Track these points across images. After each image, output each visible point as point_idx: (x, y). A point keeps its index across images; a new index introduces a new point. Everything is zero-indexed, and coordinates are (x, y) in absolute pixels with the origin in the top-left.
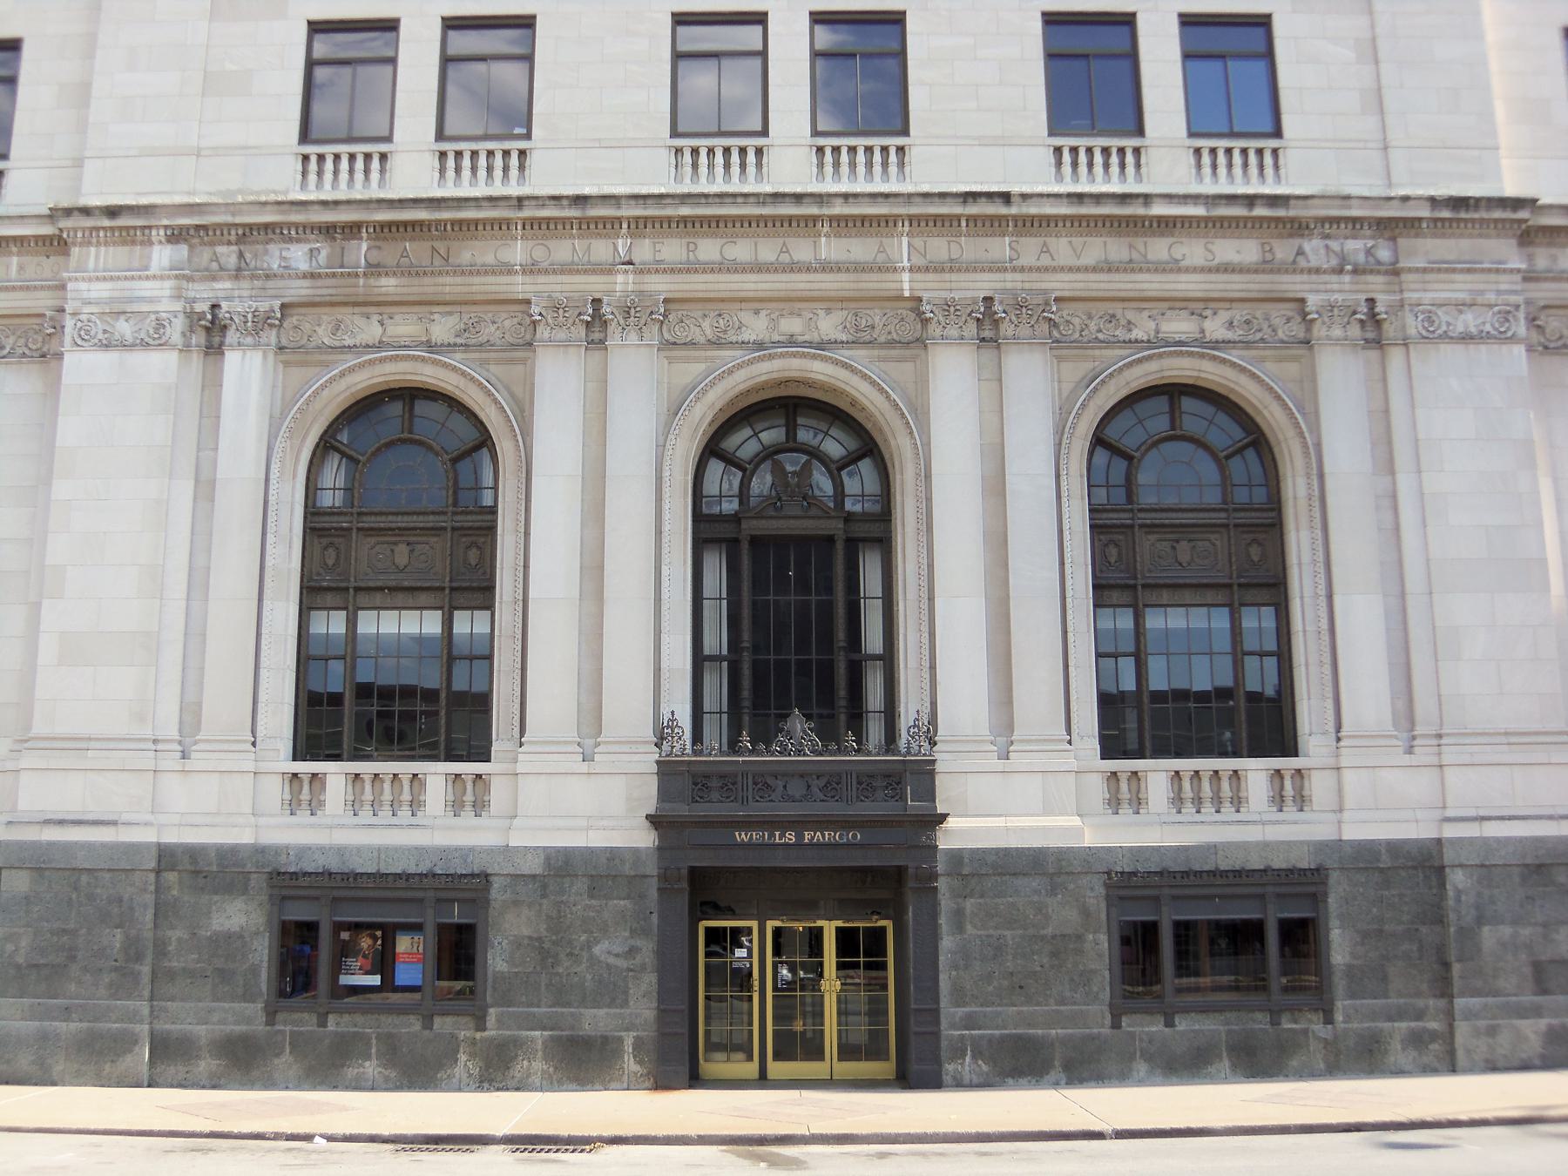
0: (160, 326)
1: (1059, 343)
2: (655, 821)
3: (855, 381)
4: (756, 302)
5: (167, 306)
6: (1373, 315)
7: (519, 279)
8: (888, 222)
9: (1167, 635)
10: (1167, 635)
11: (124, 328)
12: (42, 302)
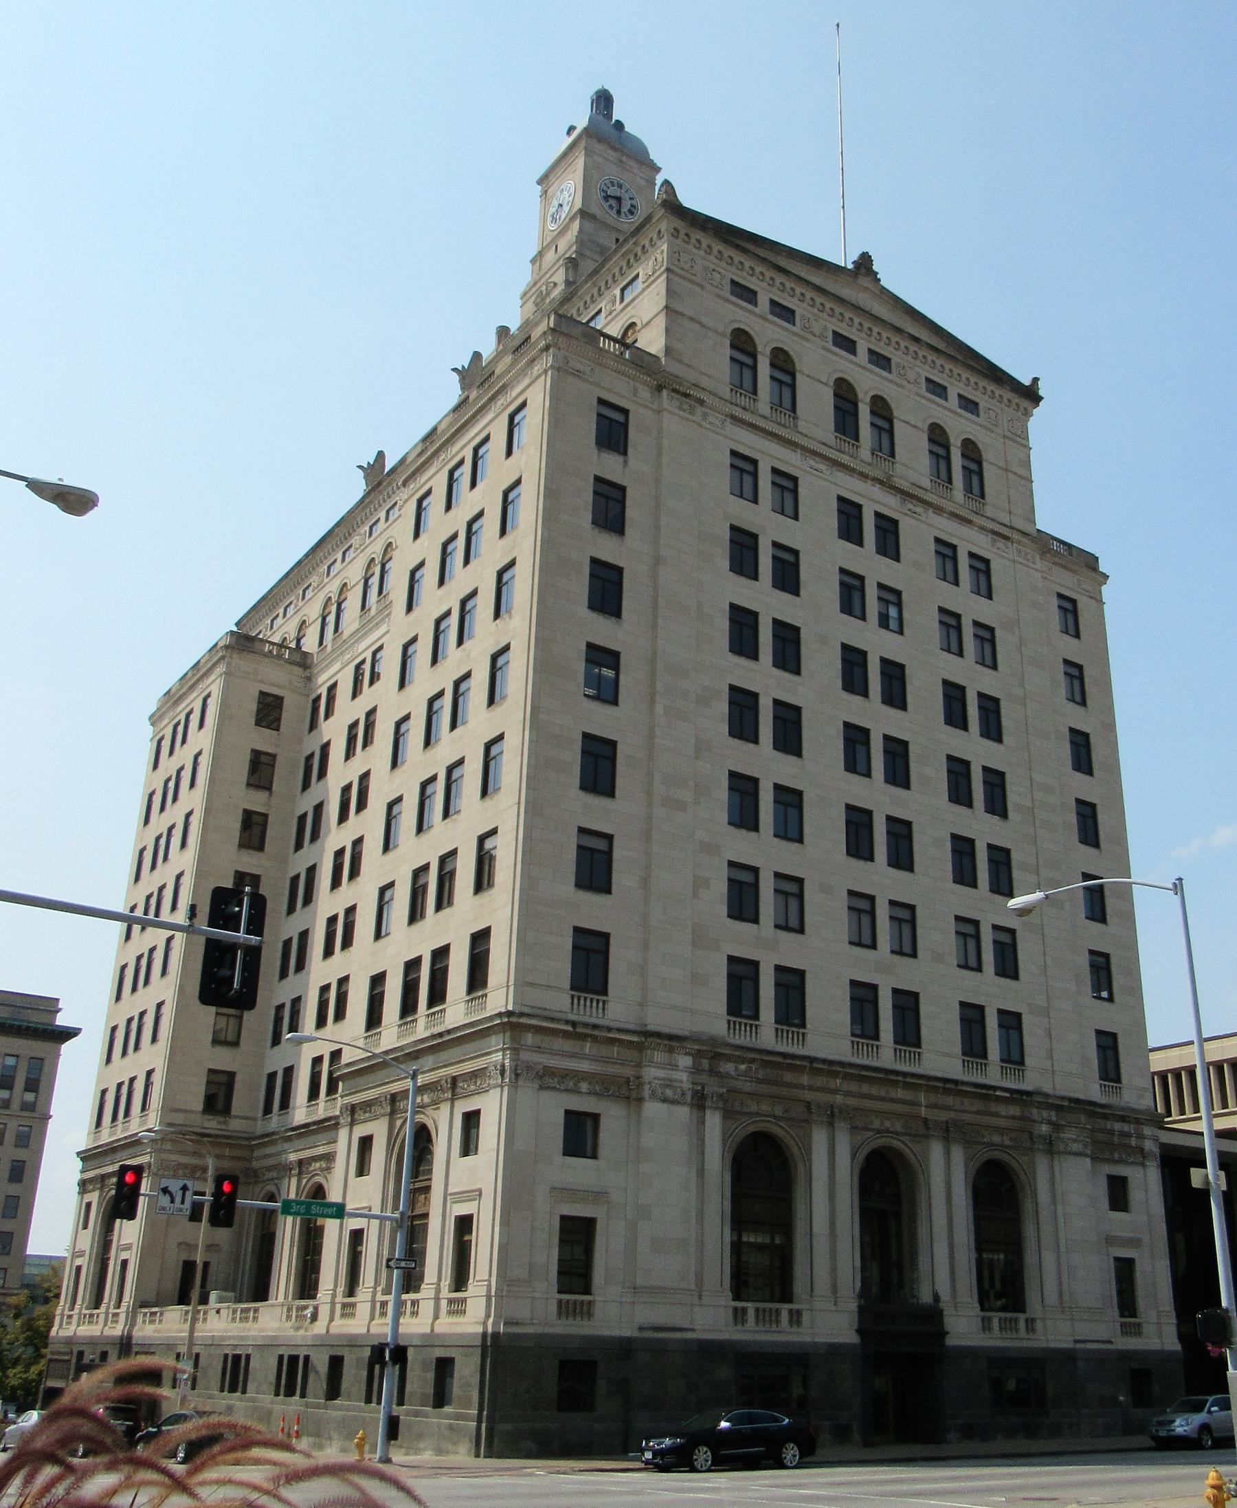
0: (683, 1094)
1: (967, 1143)
2: (860, 1331)
3: (907, 1150)
4: (877, 1113)
5: (687, 1086)
6: (1051, 1141)
7: (806, 1092)
8: (918, 1086)
9: (1099, 987)
10: (1099, 987)
11: (669, 1092)
12: (629, 1072)
